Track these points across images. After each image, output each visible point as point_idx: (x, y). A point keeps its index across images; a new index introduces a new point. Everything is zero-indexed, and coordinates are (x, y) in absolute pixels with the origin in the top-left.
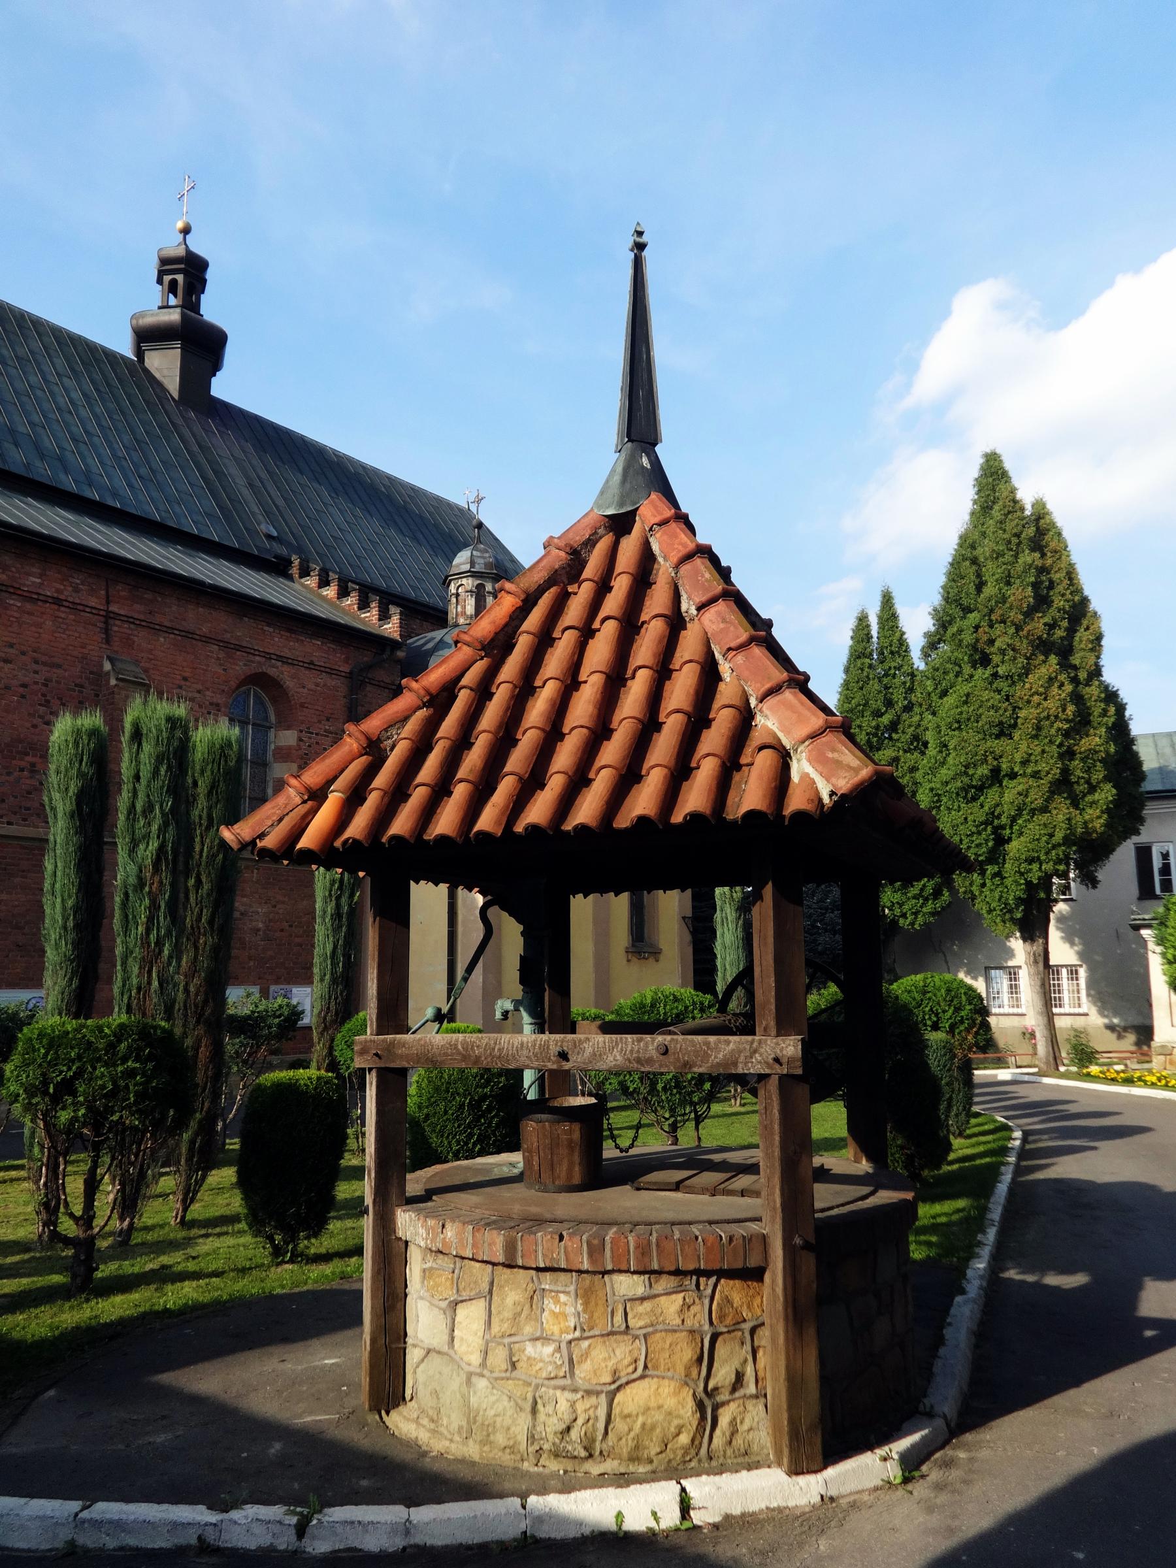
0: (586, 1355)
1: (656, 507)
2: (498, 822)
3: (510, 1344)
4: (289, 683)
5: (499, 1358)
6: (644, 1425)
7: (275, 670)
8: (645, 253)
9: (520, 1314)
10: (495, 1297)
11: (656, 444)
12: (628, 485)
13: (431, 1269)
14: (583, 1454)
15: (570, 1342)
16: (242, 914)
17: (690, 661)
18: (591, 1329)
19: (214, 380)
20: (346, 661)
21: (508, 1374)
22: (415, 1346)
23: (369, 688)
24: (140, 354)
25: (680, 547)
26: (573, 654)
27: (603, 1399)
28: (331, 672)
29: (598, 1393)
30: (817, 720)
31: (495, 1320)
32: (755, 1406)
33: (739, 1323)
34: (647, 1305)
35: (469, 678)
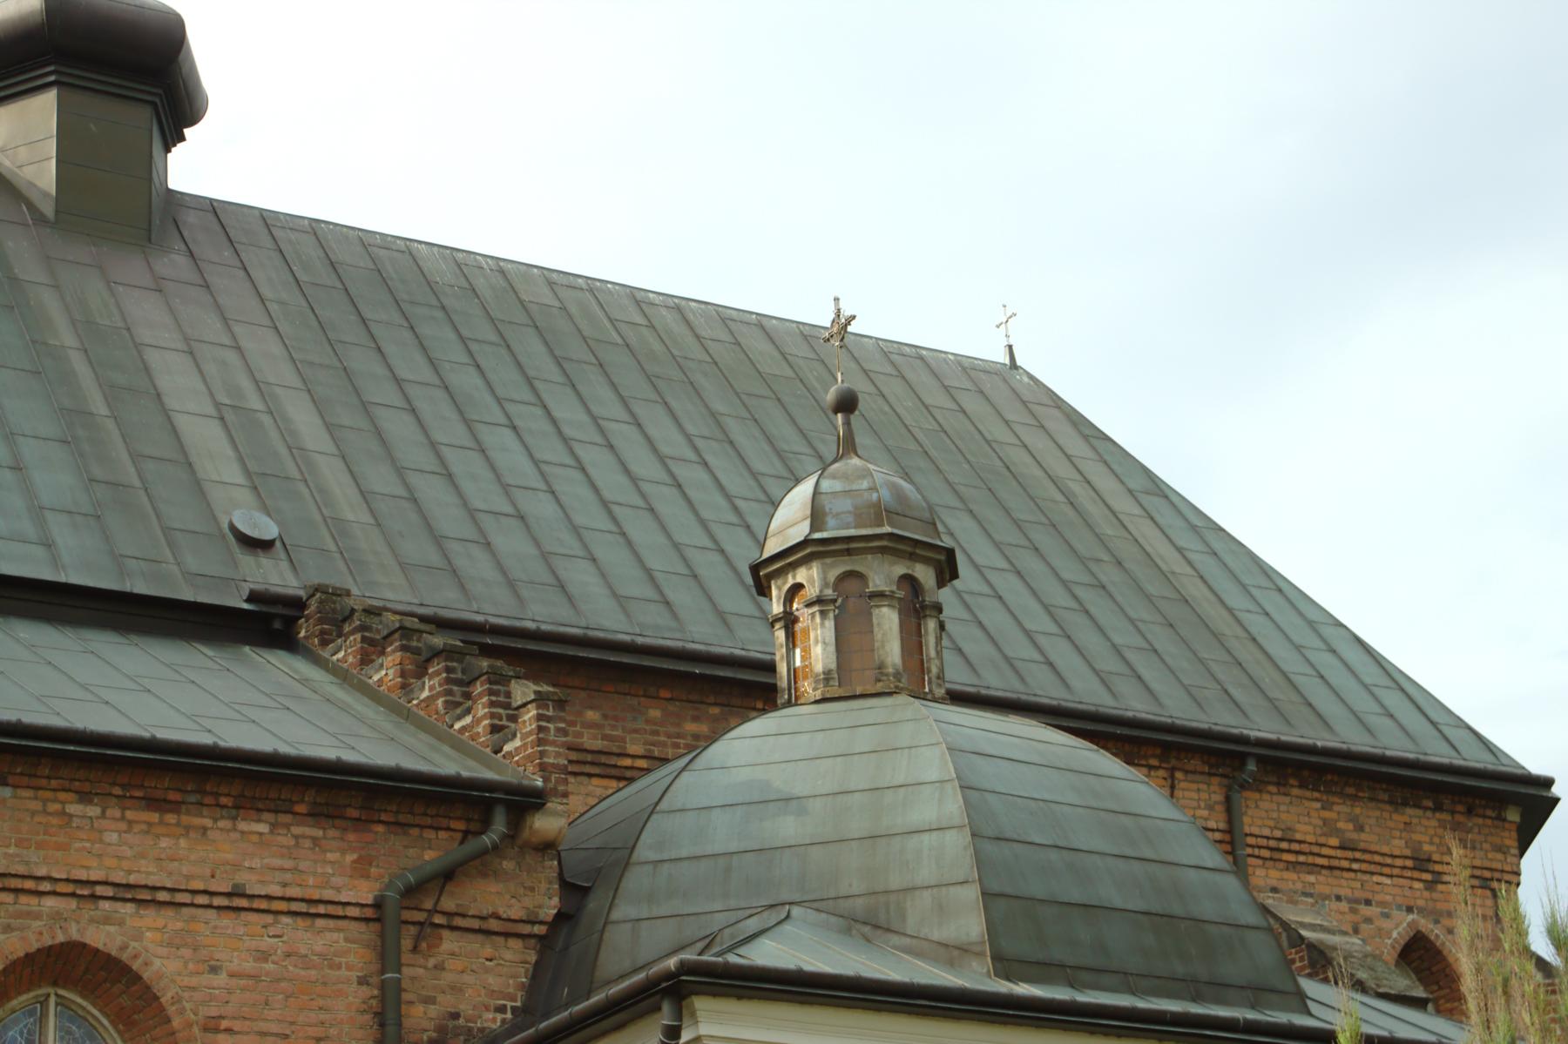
7: (104, 931)
20: (362, 868)
28: (311, 910)
30: (459, 836)
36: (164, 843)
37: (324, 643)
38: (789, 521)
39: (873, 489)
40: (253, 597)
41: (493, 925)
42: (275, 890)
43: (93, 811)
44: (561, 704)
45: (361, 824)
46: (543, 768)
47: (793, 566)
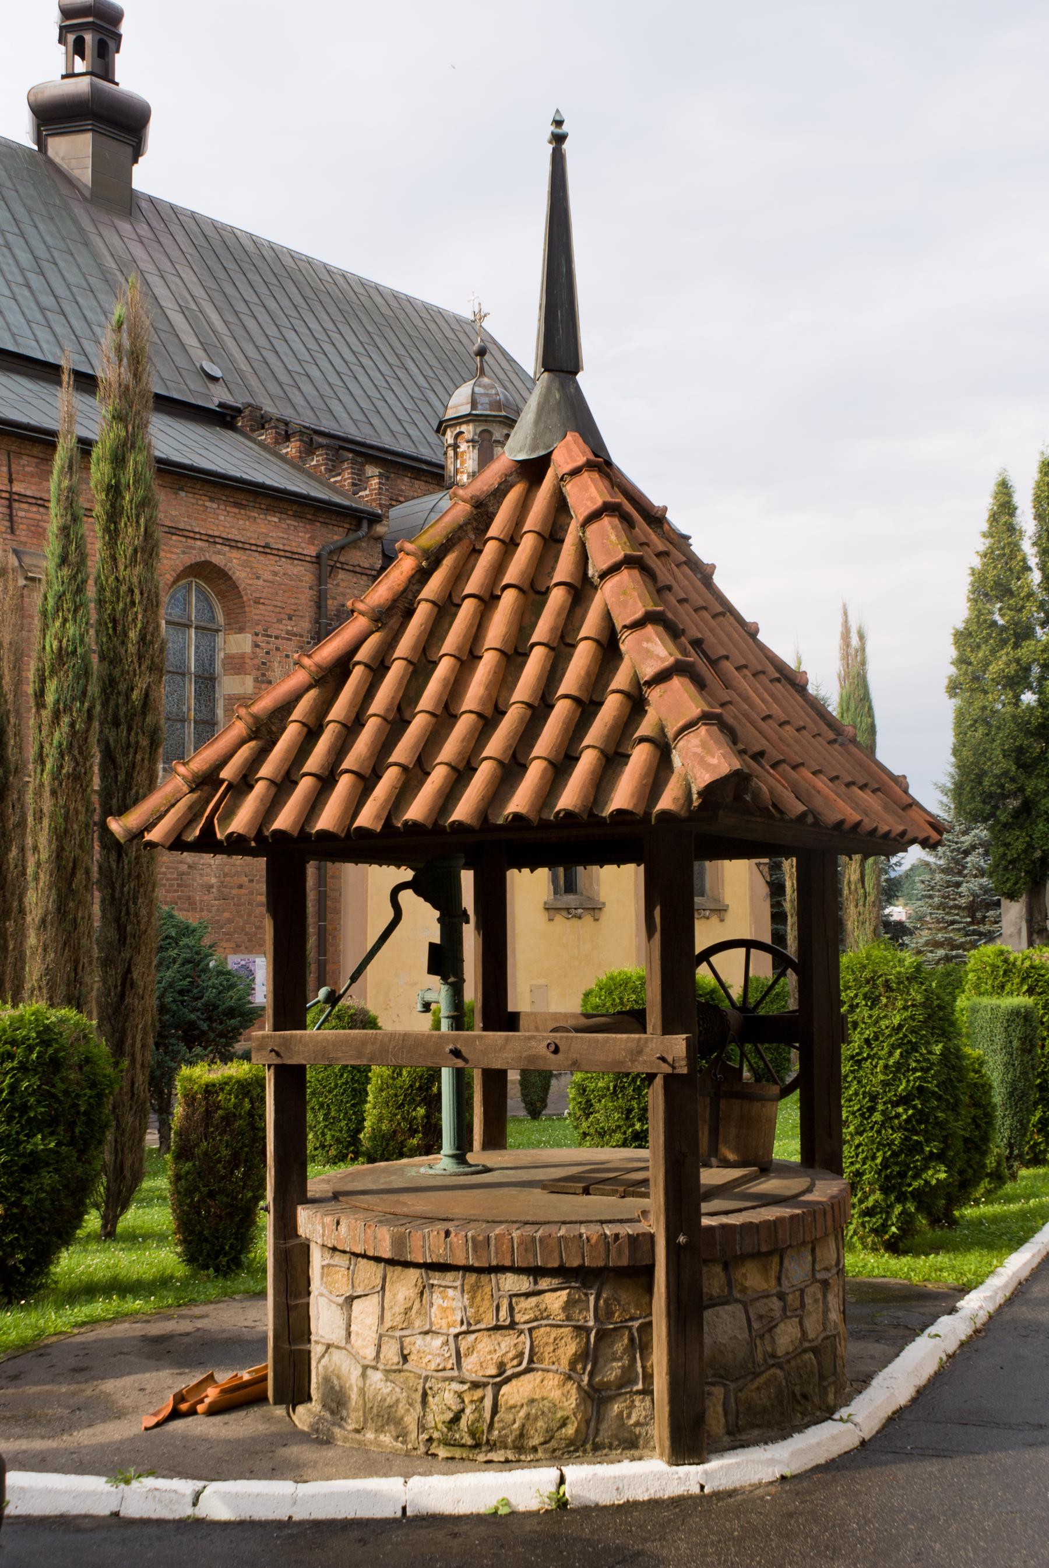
0: (471, 1350)
1: (569, 451)
2: (378, 817)
3: (401, 1337)
4: (240, 575)
5: (391, 1353)
6: (528, 1414)
7: (221, 557)
8: (566, 146)
9: (411, 1308)
10: (387, 1293)
11: (576, 373)
12: (542, 426)
13: (329, 1265)
14: (470, 1442)
15: (457, 1336)
16: (190, 867)
17: (471, 712)
18: (478, 1322)
19: (136, 168)
20: (311, 541)
21: (399, 1367)
22: (317, 1342)
23: (341, 575)
24: (40, 141)
25: (589, 503)
26: (471, 625)
27: (489, 1391)
28: (293, 556)
29: (485, 1385)
31: (388, 1315)
32: (643, 1400)
33: (626, 1321)
34: (533, 1301)
35: (299, 712)
36: (241, 522)
37: (253, 431)
38: (459, 402)
39: (497, 394)
40: (220, 405)
41: (357, 569)
42: (281, 547)
43: (215, 506)
44: (387, 478)
45: (312, 521)
46: (380, 505)
47: (461, 424)
